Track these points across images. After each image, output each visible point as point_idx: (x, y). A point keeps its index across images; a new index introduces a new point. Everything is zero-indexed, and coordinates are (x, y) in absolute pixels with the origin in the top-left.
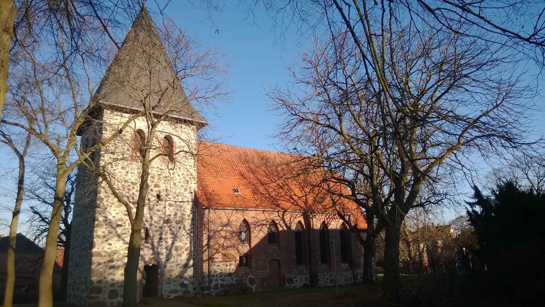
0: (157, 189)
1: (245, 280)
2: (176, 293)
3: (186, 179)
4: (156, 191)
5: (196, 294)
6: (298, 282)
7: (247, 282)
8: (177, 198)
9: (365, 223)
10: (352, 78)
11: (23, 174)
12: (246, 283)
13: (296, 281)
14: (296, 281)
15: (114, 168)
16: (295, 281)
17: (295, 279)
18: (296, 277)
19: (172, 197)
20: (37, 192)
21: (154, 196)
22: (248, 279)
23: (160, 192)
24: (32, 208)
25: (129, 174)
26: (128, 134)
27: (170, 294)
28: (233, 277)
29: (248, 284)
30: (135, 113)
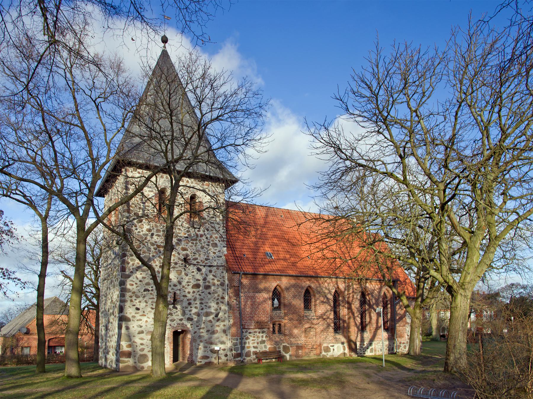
0: (184, 252)
1: (279, 348)
2: (207, 359)
3: (215, 242)
4: (183, 255)
5: (227, 360)
6: (336, 350)
7: (281, 350)
8: (206, 262)
9: (151, 279)
10: (118, 135)
11: (47, 236)
12: (280, 351)
13: (334, 350)
14: (334, 350)
15: (138, 230)
16: (332, 350)
17: (332, 348)
18: (333, 346)
19: (200, 261)
20: (66, 256)
21: (182, 260)
22: (282, 347)
23: (187, 255)
24: (62, 272)
25: (154, 236)
26: (149, 192)
27: (373, 375)
28: (266, 344)
29: (282, 351)
30: (156, 171)
